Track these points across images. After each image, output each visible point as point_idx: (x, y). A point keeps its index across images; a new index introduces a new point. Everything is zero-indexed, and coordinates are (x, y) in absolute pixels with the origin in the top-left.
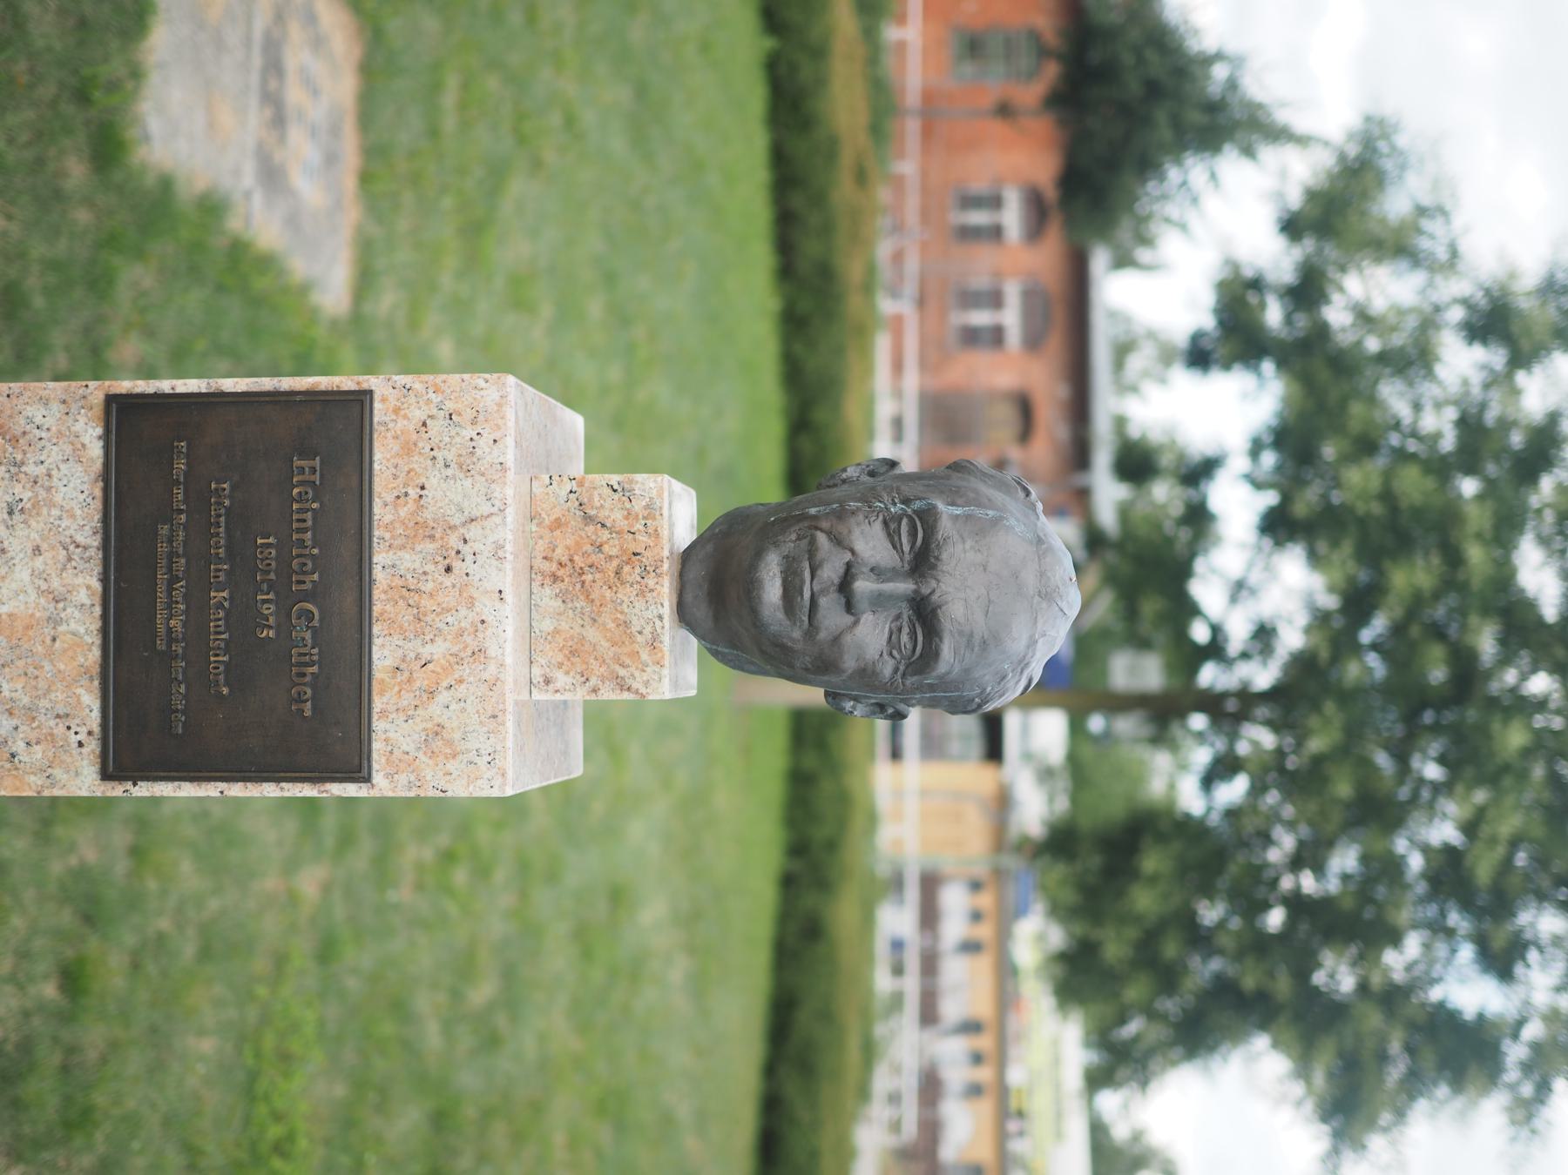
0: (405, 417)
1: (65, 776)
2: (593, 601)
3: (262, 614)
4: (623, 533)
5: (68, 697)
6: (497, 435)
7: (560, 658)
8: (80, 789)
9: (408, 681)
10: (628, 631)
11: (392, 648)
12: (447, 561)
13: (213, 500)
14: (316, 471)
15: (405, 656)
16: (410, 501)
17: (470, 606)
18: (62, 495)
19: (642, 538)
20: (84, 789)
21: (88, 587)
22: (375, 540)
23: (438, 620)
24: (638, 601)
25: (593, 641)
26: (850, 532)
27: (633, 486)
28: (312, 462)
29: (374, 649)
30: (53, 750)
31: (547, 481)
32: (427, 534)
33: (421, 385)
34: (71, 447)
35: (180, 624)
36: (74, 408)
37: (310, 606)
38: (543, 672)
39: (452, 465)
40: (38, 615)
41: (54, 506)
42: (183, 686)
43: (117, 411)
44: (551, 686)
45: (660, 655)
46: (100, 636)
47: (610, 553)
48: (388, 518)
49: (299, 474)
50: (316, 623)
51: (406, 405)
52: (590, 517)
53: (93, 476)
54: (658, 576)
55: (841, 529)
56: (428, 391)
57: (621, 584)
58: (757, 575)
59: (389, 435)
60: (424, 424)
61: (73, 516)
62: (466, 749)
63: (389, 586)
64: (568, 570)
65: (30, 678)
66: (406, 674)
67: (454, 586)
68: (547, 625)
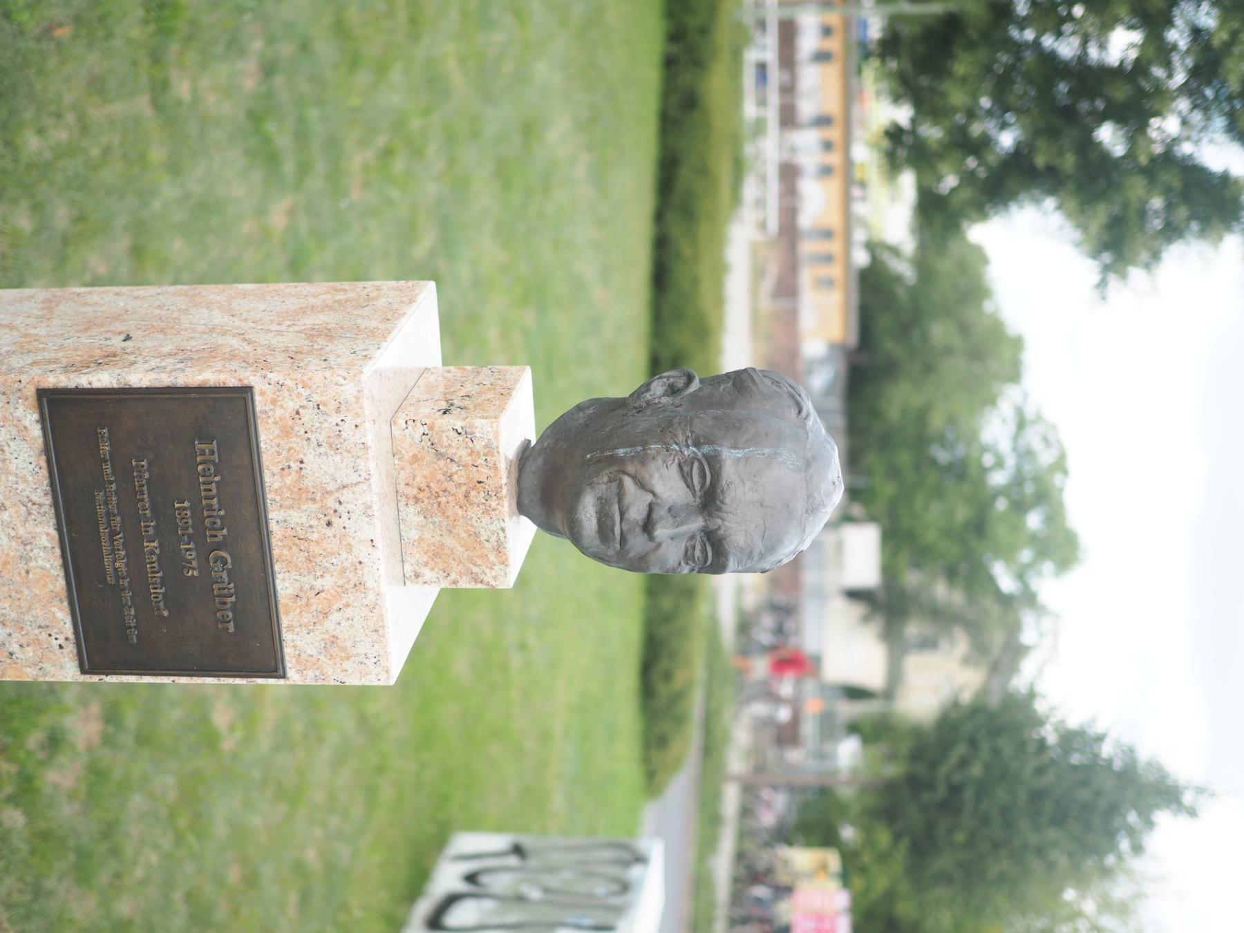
0: (281, 406)
1: (53, 669)
2: (448, 517)
3: (186, 559)
5: (46, 613)
6: (358, 421)
7: (425, 558)
8: (66, 678)
9: (307, 605)
10: (478, 540)
11: (291, 581)
12: (327, 518)
13: (135, 474)
14: (214, 452)
15: (302, 587)
16: (293, 473)
17: (348, 551)
18: (15, 465)
19: (484, 470)
20: (68, 678)
21: (48, 535)
22: (268, 501)
23: (324, 561)
24: (484, 517)
25: (451, 547)
26: (651, 476)
27: (474, 430)
28: (210, 445)
29: (278, 582)
30: (41, 650)
31: (404, 426)
32: (309, 497)
33: (291, 381)
34: (16, 429)
35: (123, 565)
36: (13, 398)
37: (224, 554)
38: (413, 569)
39: (324, 444)
40: (12, 554)
41: (10, 473)
42: (133, 610)
43: (48, 404)
44: (420, 579)
45: (504, 557)
46: (63, 570)
47: (459, 481)
48: (276, 485)
49: (201, 455)
50: (229, 566)
51: (281, 398)
52: (441, 454)
53: (37, 452)
54: (499, 499)
55: (644, 474)
56: (298, 386)
57: (470, 505)
58: (577, 516)
59: (270, 421)
60: (298, 413)
61: (26, 481)
62: (357, 654)
63: (283, 536)
64: (427, 493)
65: (14, 599)
66: (304, 600)
67: (335, 536)
68: (414, 534)
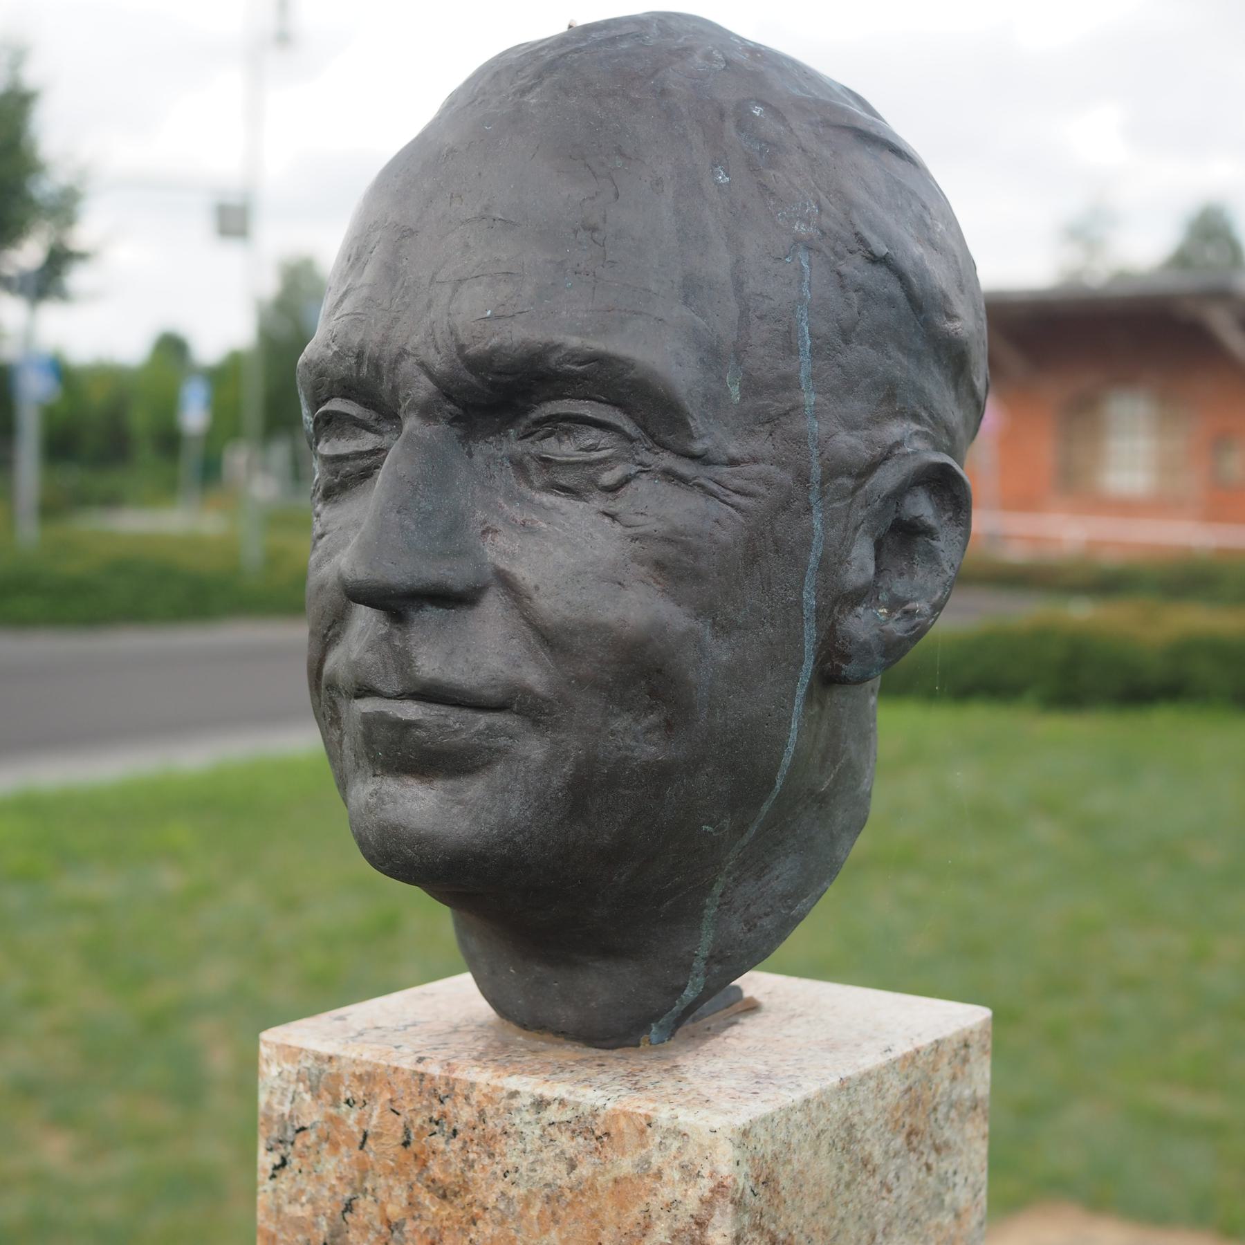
4: (365, 1163)
10: (569, 1196)
19: (376, 1115)
27: (275, 1115)
47: (404, 1203)
57: (467, 1191)
